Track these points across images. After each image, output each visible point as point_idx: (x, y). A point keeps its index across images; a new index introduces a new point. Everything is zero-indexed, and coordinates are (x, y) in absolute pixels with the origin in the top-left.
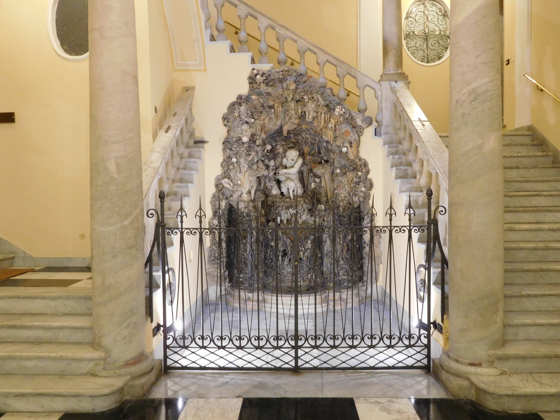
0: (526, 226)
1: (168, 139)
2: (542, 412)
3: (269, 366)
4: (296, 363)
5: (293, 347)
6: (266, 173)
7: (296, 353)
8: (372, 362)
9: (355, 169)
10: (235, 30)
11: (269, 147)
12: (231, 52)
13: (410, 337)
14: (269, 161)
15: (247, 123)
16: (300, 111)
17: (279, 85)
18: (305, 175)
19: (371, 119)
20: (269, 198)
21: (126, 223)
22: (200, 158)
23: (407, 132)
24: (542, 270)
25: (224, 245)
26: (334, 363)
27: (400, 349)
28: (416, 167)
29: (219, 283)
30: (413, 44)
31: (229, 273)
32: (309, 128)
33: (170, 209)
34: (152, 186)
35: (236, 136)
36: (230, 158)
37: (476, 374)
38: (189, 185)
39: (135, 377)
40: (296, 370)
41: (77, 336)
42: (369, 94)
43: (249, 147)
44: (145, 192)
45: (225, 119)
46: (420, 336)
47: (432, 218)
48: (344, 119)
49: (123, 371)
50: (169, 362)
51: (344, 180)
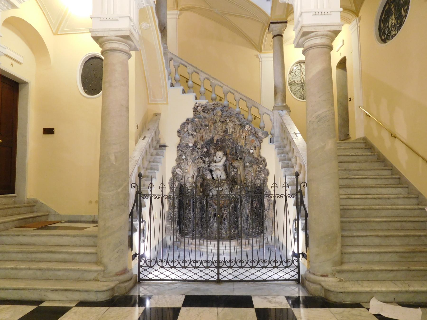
0: (358, 196)
1: (144, 144)
2: (363, 302)
3: (202, 279)
4: (218, 277)
5: (216, 267)
6: (203, 165)
7: (218, 271)
8: (264, 277)
9: (257, 163)
10: (186, 80)
11: (205, 150)
12: (183, 93)
13: (287, 261)
14: (205, 158)
15: (192, 135)
16: (224, 128)
17: (212, 112)
18: (227, 167)
19: (268, 133)
20: (205, 181)
21: (119, 190)
22: (163, 156)
23: (288, 141)
24: (367, 222)
25: (176, 210)
26: (241, 277)
27: (281, 269)
28: (293, 161)
29: (172, 233)
30: (294, 88)
31: (180, 228)
32: (230, 138)
33: (144, 185)
34: (134, 171)
35: (185, 142)
36: (181, 156)
37: (325, 281)
38: (156, 171)
39: (121, 283)
40: (218, 281)
41: (88, 258)
42: (266, 117)
43: (193, 149)
44: (130, 174)
45: (178, 132)
46: (293, 261)
47: (299, 189)
48: (251, 133)
49: (115, 278)
50: (142, 276)
51: (251, 170)
